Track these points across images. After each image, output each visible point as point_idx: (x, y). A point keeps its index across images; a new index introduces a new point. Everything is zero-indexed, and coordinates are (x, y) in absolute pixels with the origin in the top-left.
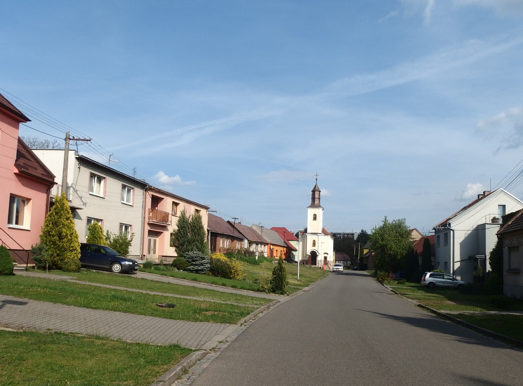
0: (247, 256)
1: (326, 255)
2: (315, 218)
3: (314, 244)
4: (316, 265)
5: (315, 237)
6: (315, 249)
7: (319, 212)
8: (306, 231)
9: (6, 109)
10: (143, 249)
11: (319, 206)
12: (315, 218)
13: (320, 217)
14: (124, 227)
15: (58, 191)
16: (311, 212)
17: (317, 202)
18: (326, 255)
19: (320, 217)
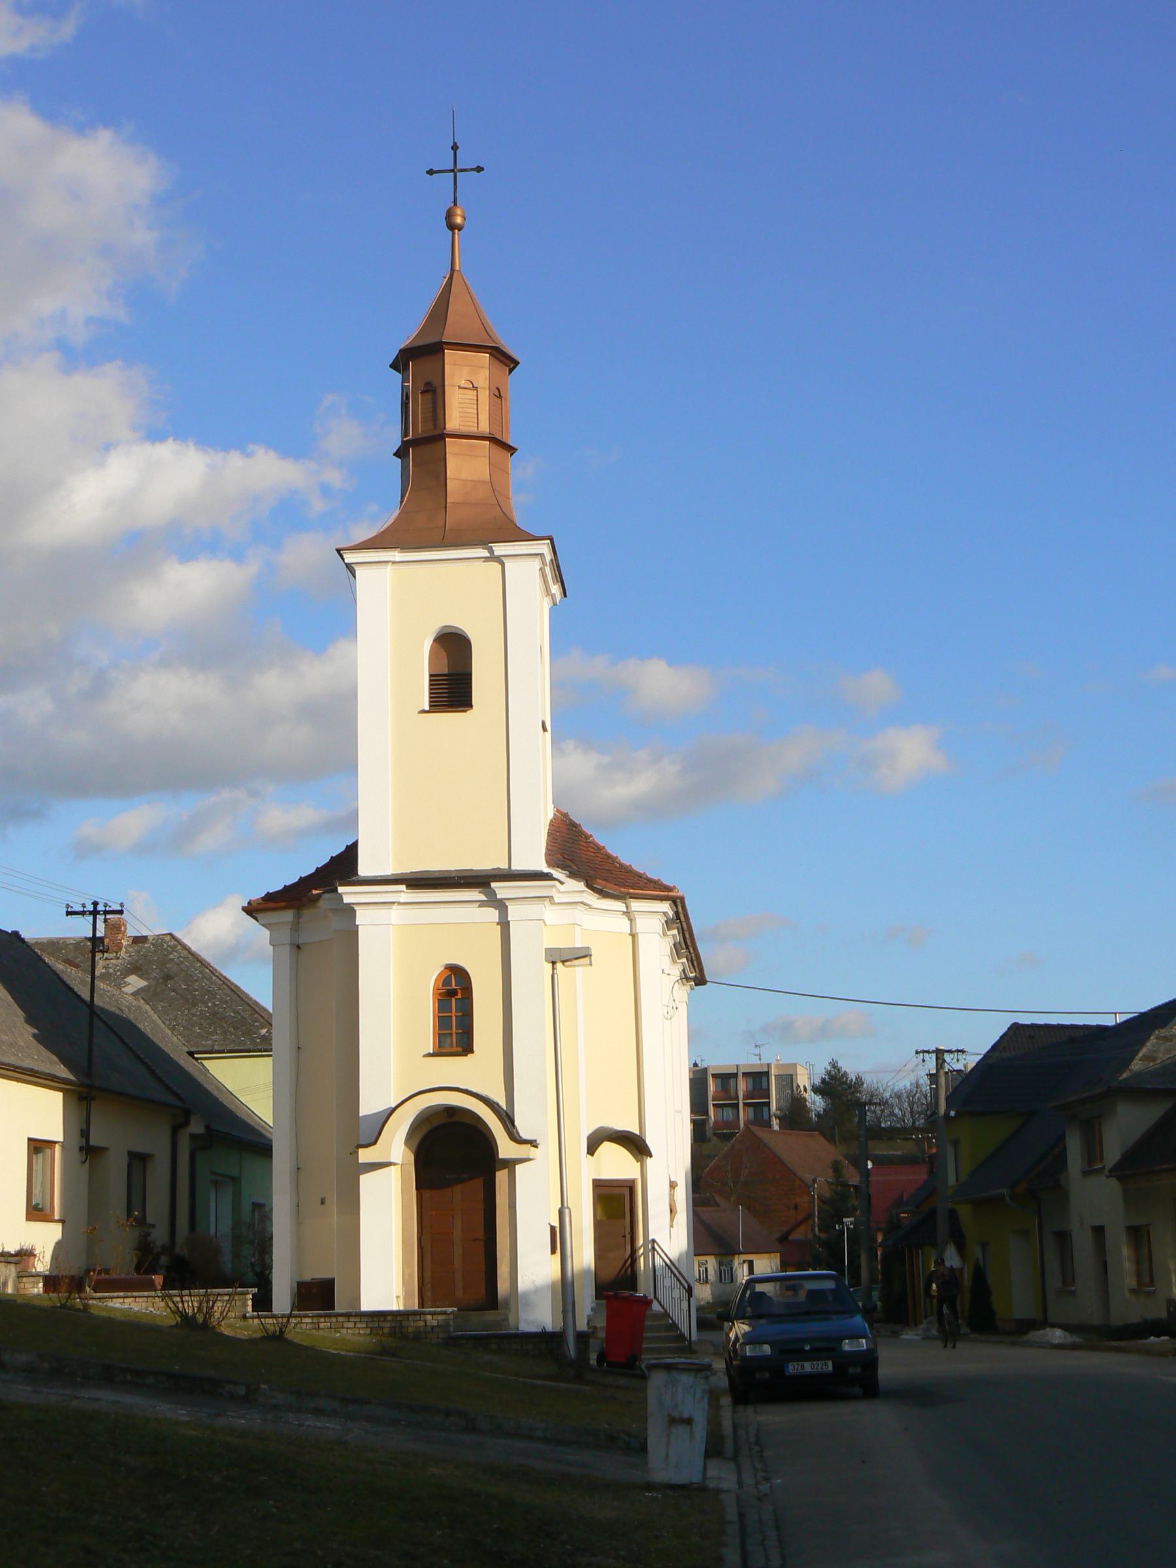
0: (200, 1308)
1: (616, 1163)
2: (452, 688)
3: (454, 1026)
4: (636, 1291)
5: (458, 930)
6: (471, 1078)
7: (508, 600)
8: (343, 867)
9: (108, 1376)
10: (1106, 1293)
11: (492, 529)
12: (452, 688)
13: (521, 667)
14: (729, 1448)
15: (118, 1297)
16: (399, 602)
17: (464, 467)
18: (616, 1163)
19: (521, 667)
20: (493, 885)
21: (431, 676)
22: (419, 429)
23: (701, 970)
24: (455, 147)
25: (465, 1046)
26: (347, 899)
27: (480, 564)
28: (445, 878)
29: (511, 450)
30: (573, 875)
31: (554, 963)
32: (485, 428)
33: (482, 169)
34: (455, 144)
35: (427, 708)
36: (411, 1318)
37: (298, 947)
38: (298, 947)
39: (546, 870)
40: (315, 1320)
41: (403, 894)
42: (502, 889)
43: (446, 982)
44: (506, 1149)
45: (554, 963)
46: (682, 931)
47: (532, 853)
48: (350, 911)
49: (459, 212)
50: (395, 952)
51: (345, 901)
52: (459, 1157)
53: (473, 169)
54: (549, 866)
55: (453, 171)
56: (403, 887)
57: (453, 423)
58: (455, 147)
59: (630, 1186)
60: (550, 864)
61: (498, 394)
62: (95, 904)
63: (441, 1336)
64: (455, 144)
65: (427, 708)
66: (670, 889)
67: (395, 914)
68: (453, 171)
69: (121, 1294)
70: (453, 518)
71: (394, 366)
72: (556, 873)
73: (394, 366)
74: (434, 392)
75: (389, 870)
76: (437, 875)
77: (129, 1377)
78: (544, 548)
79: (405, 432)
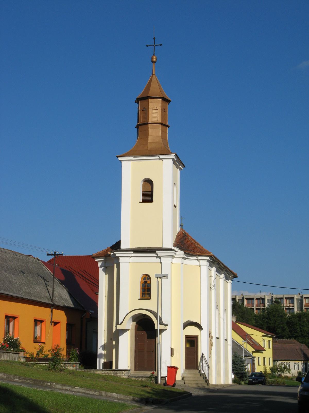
1: (192, 331)
2: (148, 196)
3: (146, 292)
5: (148, 264)
8: (117, 246)
12: (148, 196)
18: (192, 331)
20: (157, 252)
21: (143, 192)
22: (141, 122)
23: (233, 273)
24: (154, 39)
25: (149, 298)
26: (117, 255)
27: (158, 160)
28: (144, 250)
29: (168, 126)
30: (180, 249)
31: (158, 278)
32: (160, 121)
33: (162, 45)
34: (154, 38)
35: (141, 201)
36: (119, 371)
37: (106, 267)
38: (106, 267)
39: (173, 248)
40: (94, 371)
41: (131, 254)
42: (160, 253)
43: (144, 279)
44: (157, 326)
45: (158, 278)
46: (218, 264)
47: (169, 242)
48: (118, 258)
49: (154, 57)
50: (130, 270)
51: (116, 256)
52: (147, 328)
53: (159, 45)
54: (174, 246)
55: (153, 45)
56: (132, 252)
57: (150, 120)
58: (154, 39)
59: (196, 337)
60: (175, 246)
61: (164, 110)
62: (55, 252)
63: (127, 376)
64: (154, 38)
65: (141, 201)
66: (209, 253)
67: (131, 260)
68: (153, 45)
69: (45, 363)
70: (150, 147)
71: (135, 102)
72: (176, 249)
73: (135, 102)
74: (145, 110)
75: (129, 247)
76: (142, 249)
77: (24, 380)
78: (173, 156)
79: (138, 122)
